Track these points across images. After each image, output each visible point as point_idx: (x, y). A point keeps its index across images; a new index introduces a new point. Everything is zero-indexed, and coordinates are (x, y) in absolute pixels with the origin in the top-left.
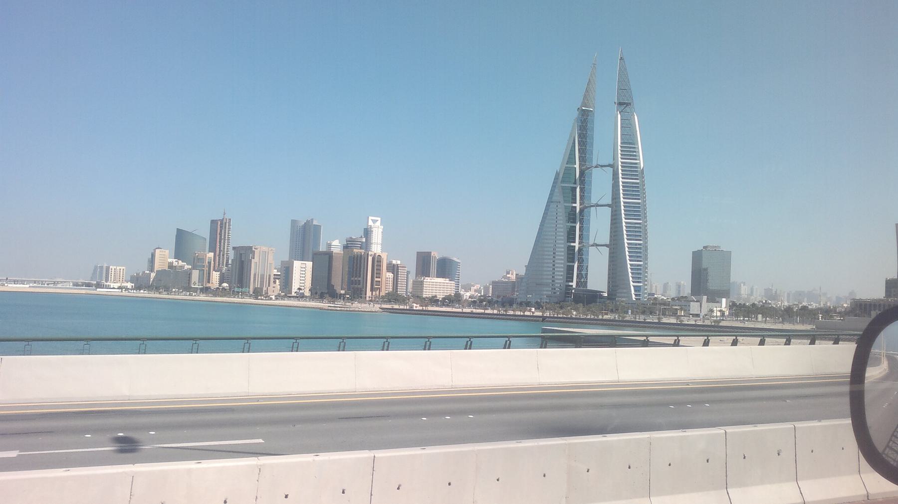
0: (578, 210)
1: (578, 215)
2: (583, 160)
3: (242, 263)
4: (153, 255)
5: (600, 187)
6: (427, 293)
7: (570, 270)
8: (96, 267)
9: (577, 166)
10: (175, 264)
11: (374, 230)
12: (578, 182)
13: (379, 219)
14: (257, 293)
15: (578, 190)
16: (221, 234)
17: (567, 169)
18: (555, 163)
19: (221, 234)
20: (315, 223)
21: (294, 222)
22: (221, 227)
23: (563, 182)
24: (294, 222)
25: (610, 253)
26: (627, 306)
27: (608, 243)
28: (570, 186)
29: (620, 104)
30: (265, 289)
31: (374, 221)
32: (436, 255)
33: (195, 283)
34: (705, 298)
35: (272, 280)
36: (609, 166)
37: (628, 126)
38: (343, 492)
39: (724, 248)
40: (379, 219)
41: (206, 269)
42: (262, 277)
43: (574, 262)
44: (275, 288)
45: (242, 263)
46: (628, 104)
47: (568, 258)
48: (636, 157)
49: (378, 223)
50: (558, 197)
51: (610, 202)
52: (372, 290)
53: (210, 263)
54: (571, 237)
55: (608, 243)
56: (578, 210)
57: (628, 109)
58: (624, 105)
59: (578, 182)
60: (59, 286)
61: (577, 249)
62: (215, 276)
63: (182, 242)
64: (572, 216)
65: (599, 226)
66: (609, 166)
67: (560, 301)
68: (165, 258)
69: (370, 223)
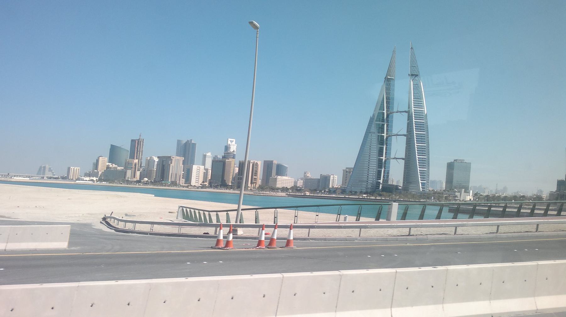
0: (385, 138)
1: (385, 141)
2: (388, 108)
3: (163, 166)
4: (98, 161)
5: (399, 124)
6: (279, 185)
7: (379, 172)
8: (41, 168)
9: (385, 112)
10: (111, 166)
11: (231, 146)
12: (385, 121)
13: (234, 140)
14: (174, 183)
15: (385, 126)
16: (137, 149)
17: (379, 113)
18: (369, 111)
19: (137, 149)
20: (193, 142)
21: (179, 142)
22: (138, 144)
23: (376, 121)
24: (179, 142)
25: (405, 163)
26: (384, 193)
27: (404, 157)
28: (380, 123)
29: (412, 75)
30: (178, 182)
31: (232, 142)
32: (275, 162)
33: (128, 178)
34: (463, 190)
35: (181, 177)
36: (405, 112)
37: (417, 87)
38: (232, 298)
39: (467, 160)
40: (234, 140)
41: (133, 169)
42: (176, 175)
43: (381, 168)
44: (182, 182)
45: (163, 166)
46: (417, 76)
47: (379, 166)
48: (422, 107)
49: (234, 143)
50: (374, 129)
51: (405, 133)
52: (251, 183)
53: (135, 165)
54: (380, 153)
55: (404, 157)
56: (385, 138)
57: (416, 78)
58: (414, 75)
59: (385, 121)
60: (34, 178)
61: (384, 160)
62: (138, 173)
63: (114, 153)
64: (381, 141)
65: (398, 147)
66: (405, 112)
67: (368, 192)
68: (104, 162)
69: (229, 142)
